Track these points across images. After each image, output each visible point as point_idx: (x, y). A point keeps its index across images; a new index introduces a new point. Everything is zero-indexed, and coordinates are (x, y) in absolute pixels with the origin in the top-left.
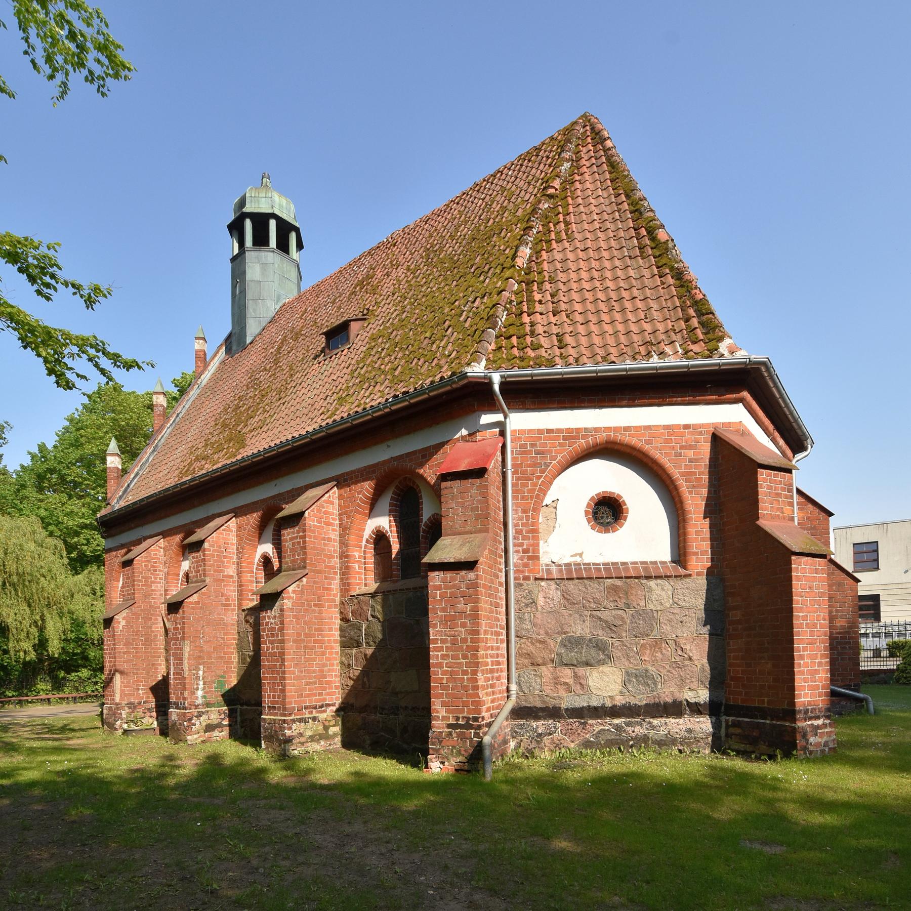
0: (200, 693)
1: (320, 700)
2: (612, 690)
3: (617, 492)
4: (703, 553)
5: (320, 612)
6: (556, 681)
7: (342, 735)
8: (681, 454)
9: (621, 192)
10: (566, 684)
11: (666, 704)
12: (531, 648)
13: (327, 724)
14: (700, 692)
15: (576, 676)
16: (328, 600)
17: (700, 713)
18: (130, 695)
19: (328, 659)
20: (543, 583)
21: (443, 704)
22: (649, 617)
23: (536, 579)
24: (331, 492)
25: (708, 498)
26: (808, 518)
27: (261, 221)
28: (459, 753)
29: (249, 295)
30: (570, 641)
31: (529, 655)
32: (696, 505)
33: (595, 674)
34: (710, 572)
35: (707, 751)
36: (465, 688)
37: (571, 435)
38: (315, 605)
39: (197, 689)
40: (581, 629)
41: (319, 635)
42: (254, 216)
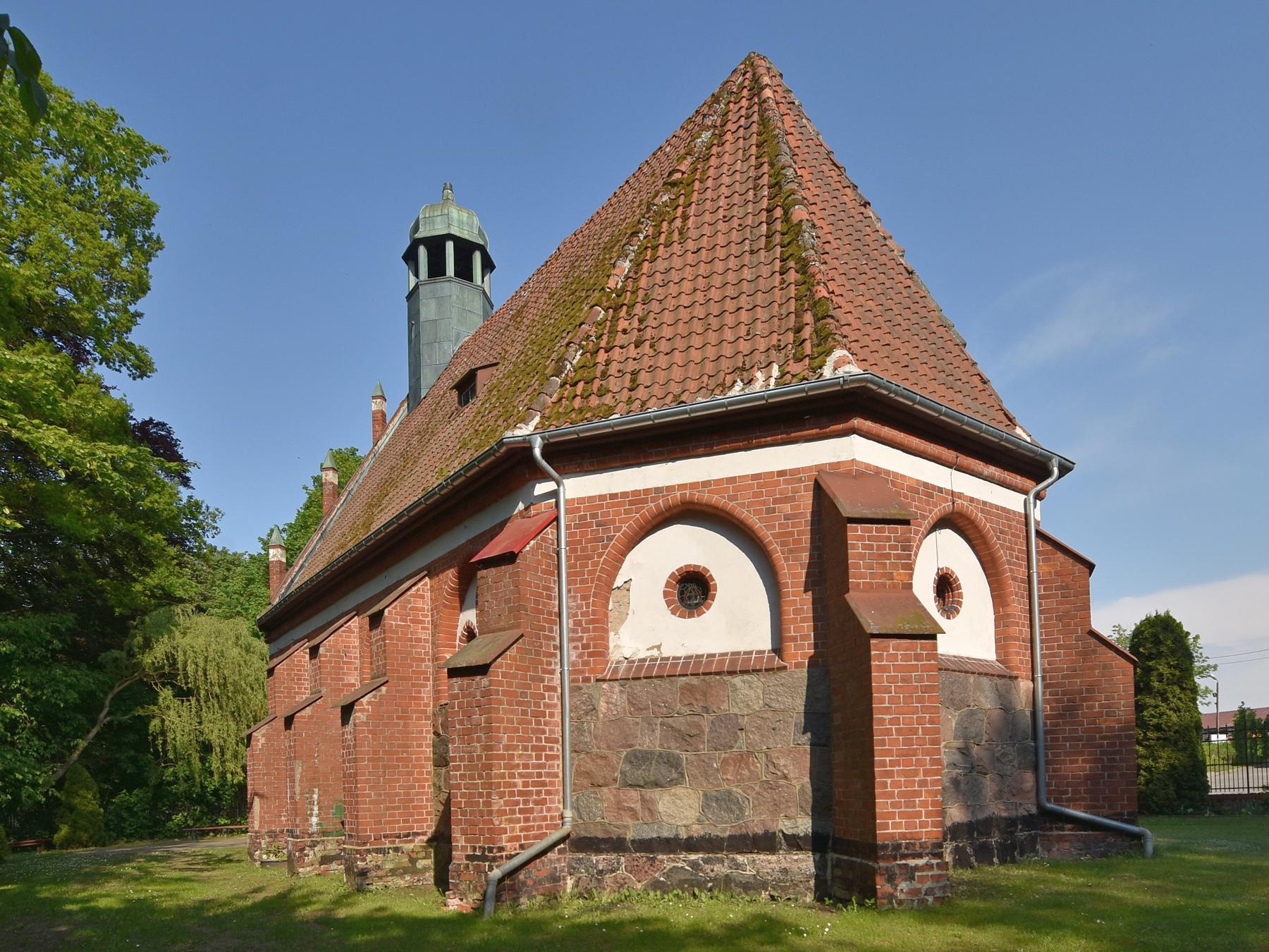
0: (314, 820)
1: (405, 828)
2: (686, 818)
3: (703, 564)
4: (804, 638)
5: (406, 726)
6: (620, 807)
7: (435, 869)
8: (774, 510)
9: (766, 159)
10: (632, 809)
11: (755, 836)
12: (590, 766)
13: (414, 855)
14: (800, 821)
15: (643, 800)
16: (416, 711)
17: (800, 848)
18: (270, 822)
19: (416, 780)
20: (605, 686)
21: (464, 832)
22: (733, 726)
23: (598, 680)
24: (420, 585)
25: (810, 565)
26: (1057, 573)
27: (436, 245)
28: (475, 889)
29: (424, 339)
30: (636, 757)
31: (588, 774)
32: (794, 576)
33: (667, 798)
34: (813, 662)
35: (809, 898)
36: (481, 813)
37: (637, 498)
38: (398, 718)
39: (311, 815)
40: (650, 741)
41: (403, 752)
42: (426, 241)
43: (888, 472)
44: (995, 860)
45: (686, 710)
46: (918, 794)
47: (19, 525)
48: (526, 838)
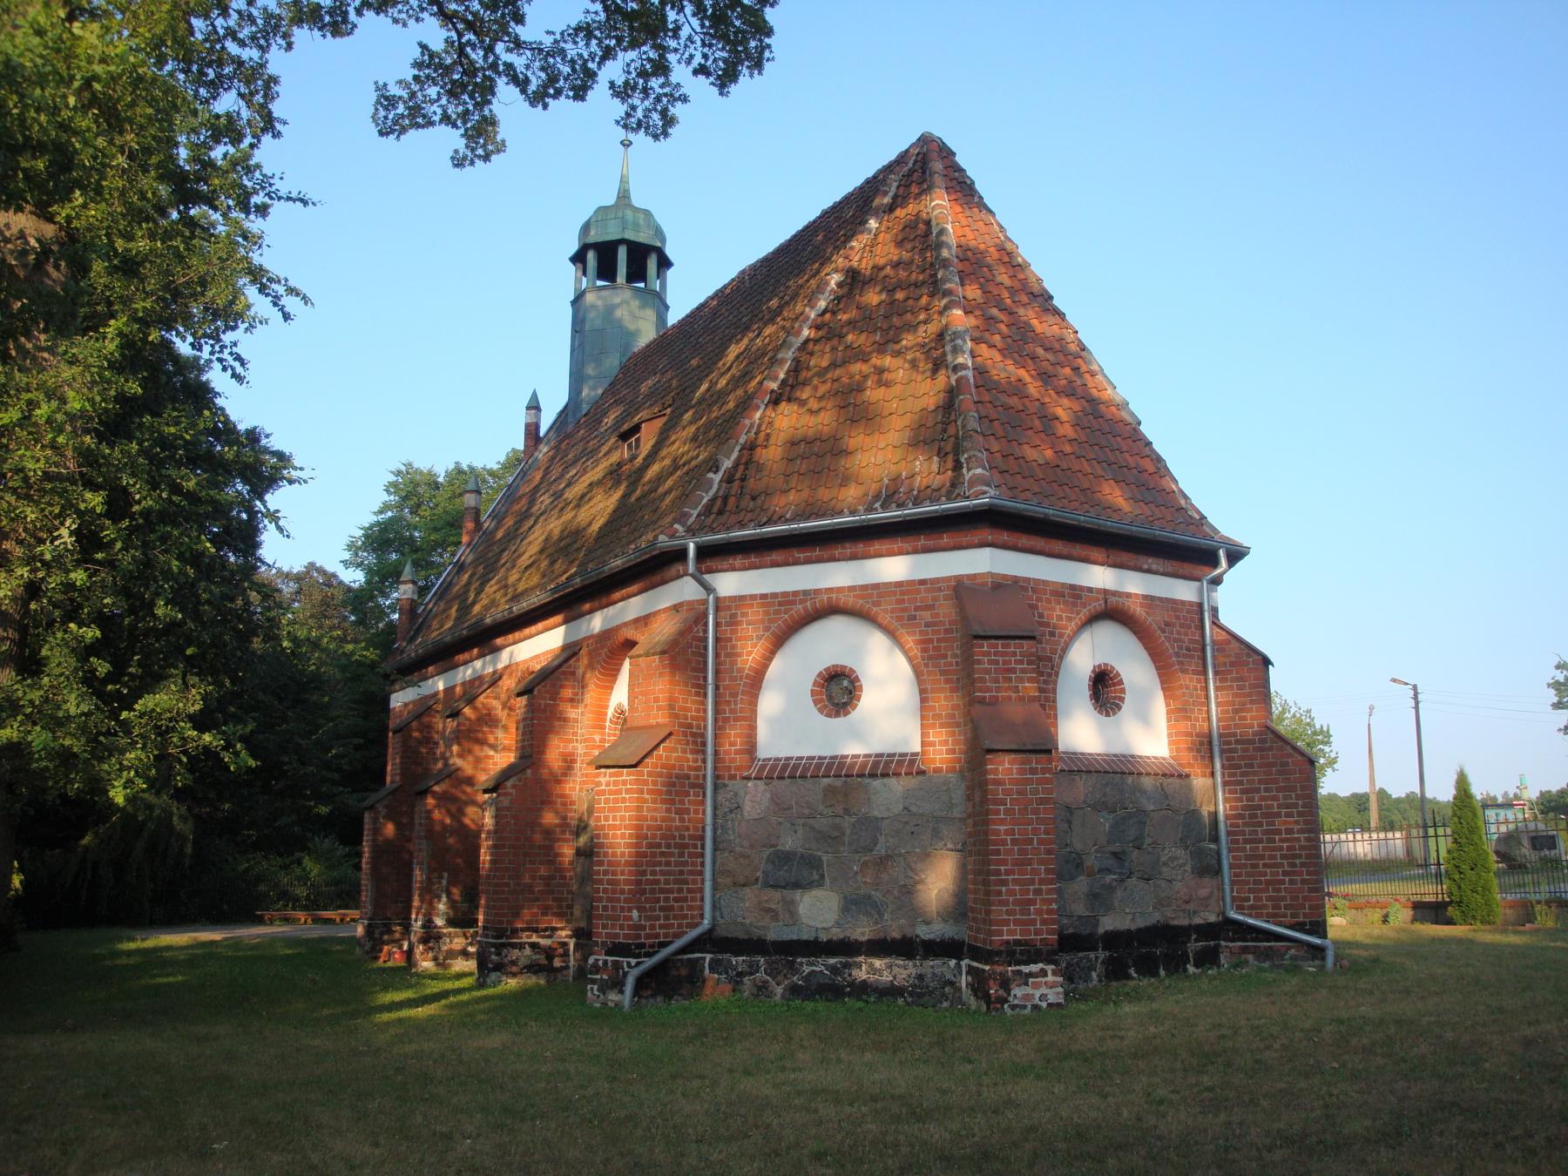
8: (914, 618)
11: (894, 941)
42: (597, 246)
43: (1028, 580)
44: (1132, 971)
45: (828, 811)
46: (1033, 902)
47: (448, 821)
48: (666, 935)
